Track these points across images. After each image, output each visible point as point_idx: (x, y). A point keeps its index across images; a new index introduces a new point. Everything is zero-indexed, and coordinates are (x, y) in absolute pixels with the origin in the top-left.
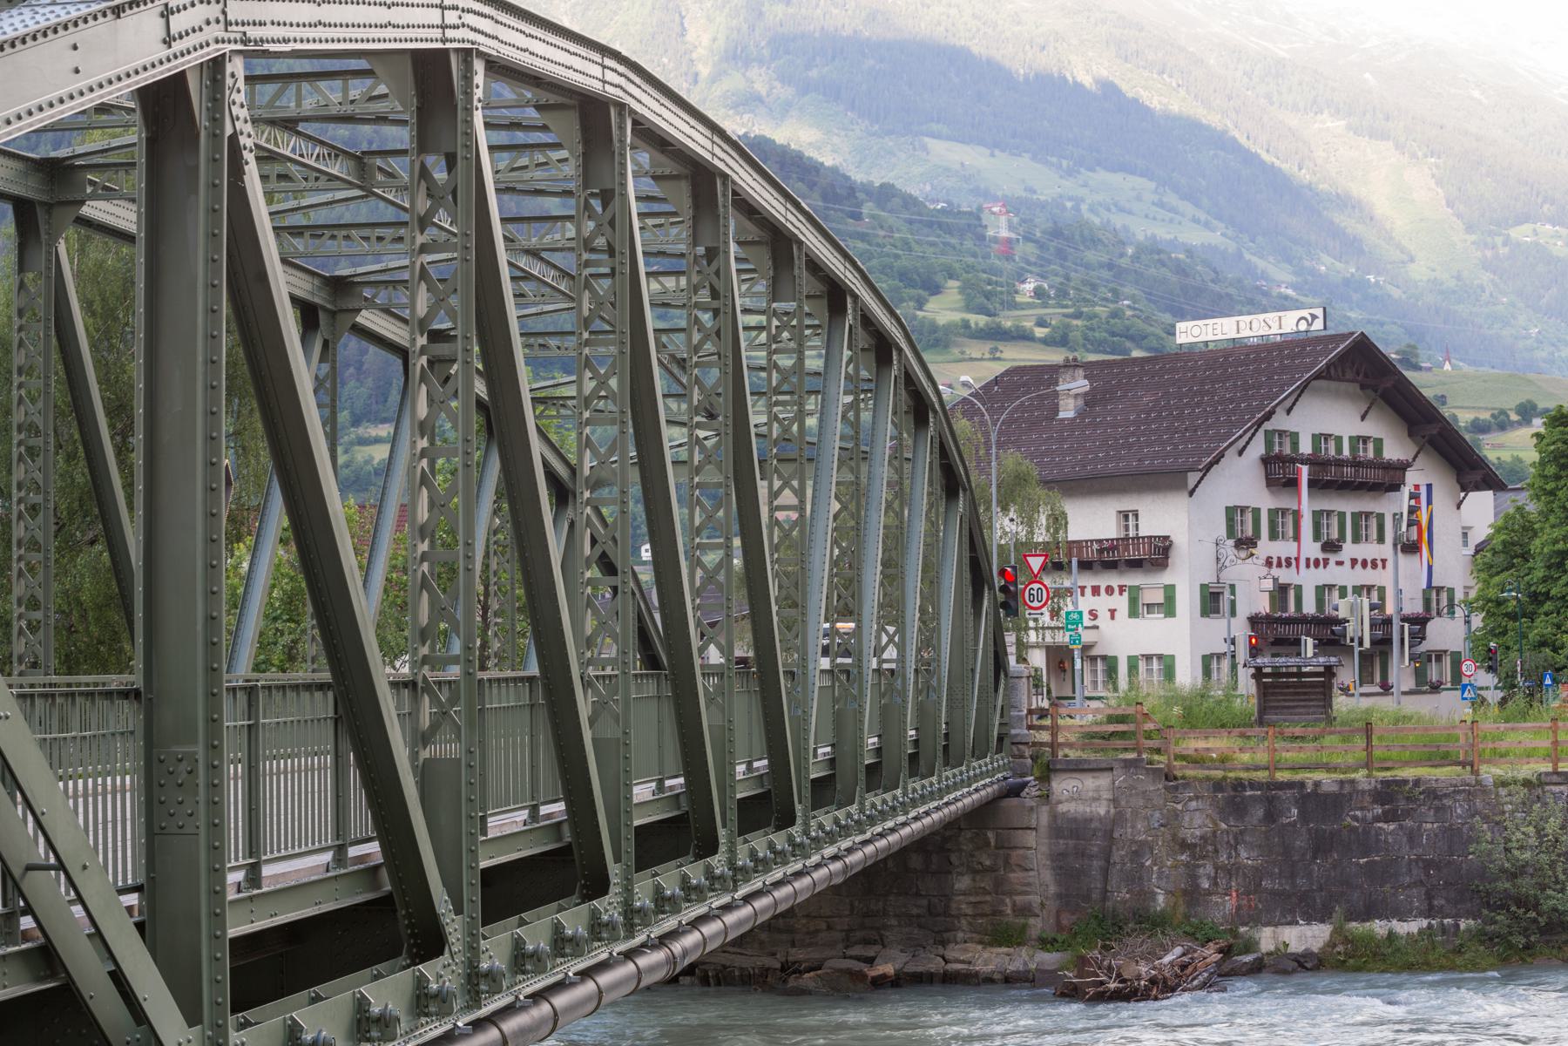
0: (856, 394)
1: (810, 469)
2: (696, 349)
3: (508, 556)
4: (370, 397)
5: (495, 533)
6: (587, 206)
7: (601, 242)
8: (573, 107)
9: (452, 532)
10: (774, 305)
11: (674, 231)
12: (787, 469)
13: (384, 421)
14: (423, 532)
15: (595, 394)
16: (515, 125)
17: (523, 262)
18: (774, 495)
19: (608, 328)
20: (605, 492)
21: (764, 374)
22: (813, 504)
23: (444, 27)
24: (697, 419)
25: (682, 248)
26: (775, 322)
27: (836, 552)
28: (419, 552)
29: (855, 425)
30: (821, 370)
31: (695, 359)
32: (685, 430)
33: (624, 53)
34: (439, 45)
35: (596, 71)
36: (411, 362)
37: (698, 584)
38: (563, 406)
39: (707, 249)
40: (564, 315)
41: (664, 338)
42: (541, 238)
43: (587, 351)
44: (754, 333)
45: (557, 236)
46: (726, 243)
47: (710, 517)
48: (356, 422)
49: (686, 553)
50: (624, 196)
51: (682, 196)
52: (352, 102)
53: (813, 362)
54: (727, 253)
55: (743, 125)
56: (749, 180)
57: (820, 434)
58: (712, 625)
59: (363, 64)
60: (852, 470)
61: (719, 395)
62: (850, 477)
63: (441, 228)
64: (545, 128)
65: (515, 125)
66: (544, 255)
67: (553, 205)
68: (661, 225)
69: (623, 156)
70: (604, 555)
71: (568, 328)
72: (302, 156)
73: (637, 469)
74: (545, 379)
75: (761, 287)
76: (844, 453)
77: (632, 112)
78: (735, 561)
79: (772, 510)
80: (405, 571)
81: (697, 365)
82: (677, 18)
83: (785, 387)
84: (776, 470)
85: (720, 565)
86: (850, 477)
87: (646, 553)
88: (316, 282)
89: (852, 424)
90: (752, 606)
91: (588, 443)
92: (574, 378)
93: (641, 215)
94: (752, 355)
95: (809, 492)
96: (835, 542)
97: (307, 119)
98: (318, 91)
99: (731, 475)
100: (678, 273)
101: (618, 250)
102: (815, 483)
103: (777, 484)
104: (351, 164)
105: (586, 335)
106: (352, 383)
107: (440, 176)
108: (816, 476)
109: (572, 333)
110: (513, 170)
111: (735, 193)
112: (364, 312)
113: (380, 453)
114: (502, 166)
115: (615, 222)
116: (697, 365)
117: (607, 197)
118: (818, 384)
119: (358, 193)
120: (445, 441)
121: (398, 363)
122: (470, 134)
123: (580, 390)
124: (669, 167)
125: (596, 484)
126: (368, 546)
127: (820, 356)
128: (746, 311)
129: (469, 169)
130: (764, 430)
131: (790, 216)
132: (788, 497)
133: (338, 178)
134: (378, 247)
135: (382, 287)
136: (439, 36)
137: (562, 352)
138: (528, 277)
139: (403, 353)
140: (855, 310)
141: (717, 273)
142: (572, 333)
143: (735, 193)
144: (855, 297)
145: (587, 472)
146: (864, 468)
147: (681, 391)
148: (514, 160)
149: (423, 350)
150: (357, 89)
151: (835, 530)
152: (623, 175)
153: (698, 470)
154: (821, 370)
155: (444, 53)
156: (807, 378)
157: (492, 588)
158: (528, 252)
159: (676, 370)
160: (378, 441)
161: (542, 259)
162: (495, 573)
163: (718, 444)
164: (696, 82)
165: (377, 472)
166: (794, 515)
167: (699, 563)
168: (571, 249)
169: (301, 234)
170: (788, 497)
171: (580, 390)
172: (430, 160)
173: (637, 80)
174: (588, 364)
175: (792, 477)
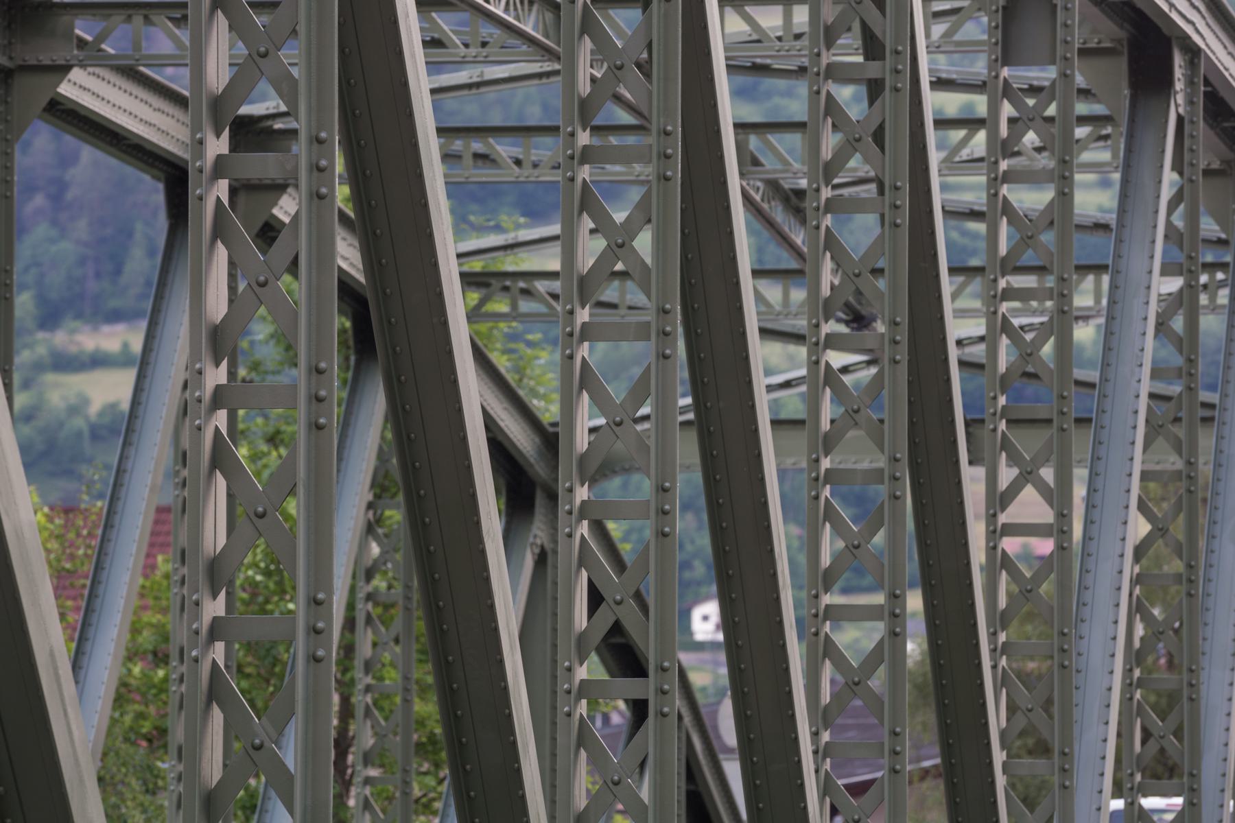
0: (1191, 275)
1: (1081, 443)
2: (829, 170)
3: (397, 626)
4: (82, 261)
5: (369, 575)
9: (278, 571)
10: (1005, 72)
12: (1029, 442)
13: (115, 316)
14: (217, 574)
15: (604, 271)
18: (999, 500)
19: (626, 118)
20: (613, 487)
21: (980, 227)
22: (1088, 522)
24: (831, 327)
26: (1007, 110)
27: (1139, 630)
28: (206, 619)
29: (1188, 343)
30: (1112, 219)
31: (826, 193)
32: (802, 352)
36: (194, 191)
37: (826, 697)
38: (526, 292)
40: (532, 86)
41: (753, 142)
43: (585, 173)
44: (958, 134)
47: (854, 548)
48: (50, 318)
49: (799, 622)
53: (1093, 199)
57: (1106, 365)
58: (858, 790)
60: (1178, 447)
61: (878, 272)
62: (1174, 462)
70: (617, 628)
71: (534, 117)
73: (693, 435)
74: (481, 230)
75: (976, 29)
76: (1161, 408)
78: (910, 646)
79: (995, 533)
80: (160, 658)
81: (830, 206)
83: (1028, 258)
84: (1006, 445)
85: (874, 659)
86: (1174, 462)
87: (705, 621)
89: (1179, 343)
90: (947, 750)
91: (587, 380)
92: (555, 229)
94: (954, 187)
95: (1079, 492)
96: (1138, 608)
99: (903, 454)
102: (1093, 475)
103: (1006, 475)
105: (584, 138)
106: (41, 230)
108: (1096, 458)
109: (554, 130)
112: (76, 74)
113: (110, 390)
116: (830, 206)
118: (1093, 251)
120: (255, 366)
121: (153, 192)
123: (569, 256)
125: (599, 468)
126: (83, 594)
127: (1105, 184)
128: (940, 84)
130: (978, 352)
132: (1030, 506)
135: (118, 18)
137: (526, 173)
139: (175, 177)
140: (1190, 82)
142: (554, 130)
144: (1193, 53)
145: (582, 441)
146: (1206, 440)
147: (794, 265)
149: (220, 168)
151: (1137, 580)
153: (829, 443)
154: (1112, 219)
156: (1077, 236)
157: (360, 700)
159: (779, 214)
160: (98, 361)
162: (368, 667)
163: (878, 379)
165: (97, 433)
166: (1045, 546)
167: (829, 650)
170: (1030, 506)
171: (569, 256)
174: (588, 202)
175: (1038, 461)
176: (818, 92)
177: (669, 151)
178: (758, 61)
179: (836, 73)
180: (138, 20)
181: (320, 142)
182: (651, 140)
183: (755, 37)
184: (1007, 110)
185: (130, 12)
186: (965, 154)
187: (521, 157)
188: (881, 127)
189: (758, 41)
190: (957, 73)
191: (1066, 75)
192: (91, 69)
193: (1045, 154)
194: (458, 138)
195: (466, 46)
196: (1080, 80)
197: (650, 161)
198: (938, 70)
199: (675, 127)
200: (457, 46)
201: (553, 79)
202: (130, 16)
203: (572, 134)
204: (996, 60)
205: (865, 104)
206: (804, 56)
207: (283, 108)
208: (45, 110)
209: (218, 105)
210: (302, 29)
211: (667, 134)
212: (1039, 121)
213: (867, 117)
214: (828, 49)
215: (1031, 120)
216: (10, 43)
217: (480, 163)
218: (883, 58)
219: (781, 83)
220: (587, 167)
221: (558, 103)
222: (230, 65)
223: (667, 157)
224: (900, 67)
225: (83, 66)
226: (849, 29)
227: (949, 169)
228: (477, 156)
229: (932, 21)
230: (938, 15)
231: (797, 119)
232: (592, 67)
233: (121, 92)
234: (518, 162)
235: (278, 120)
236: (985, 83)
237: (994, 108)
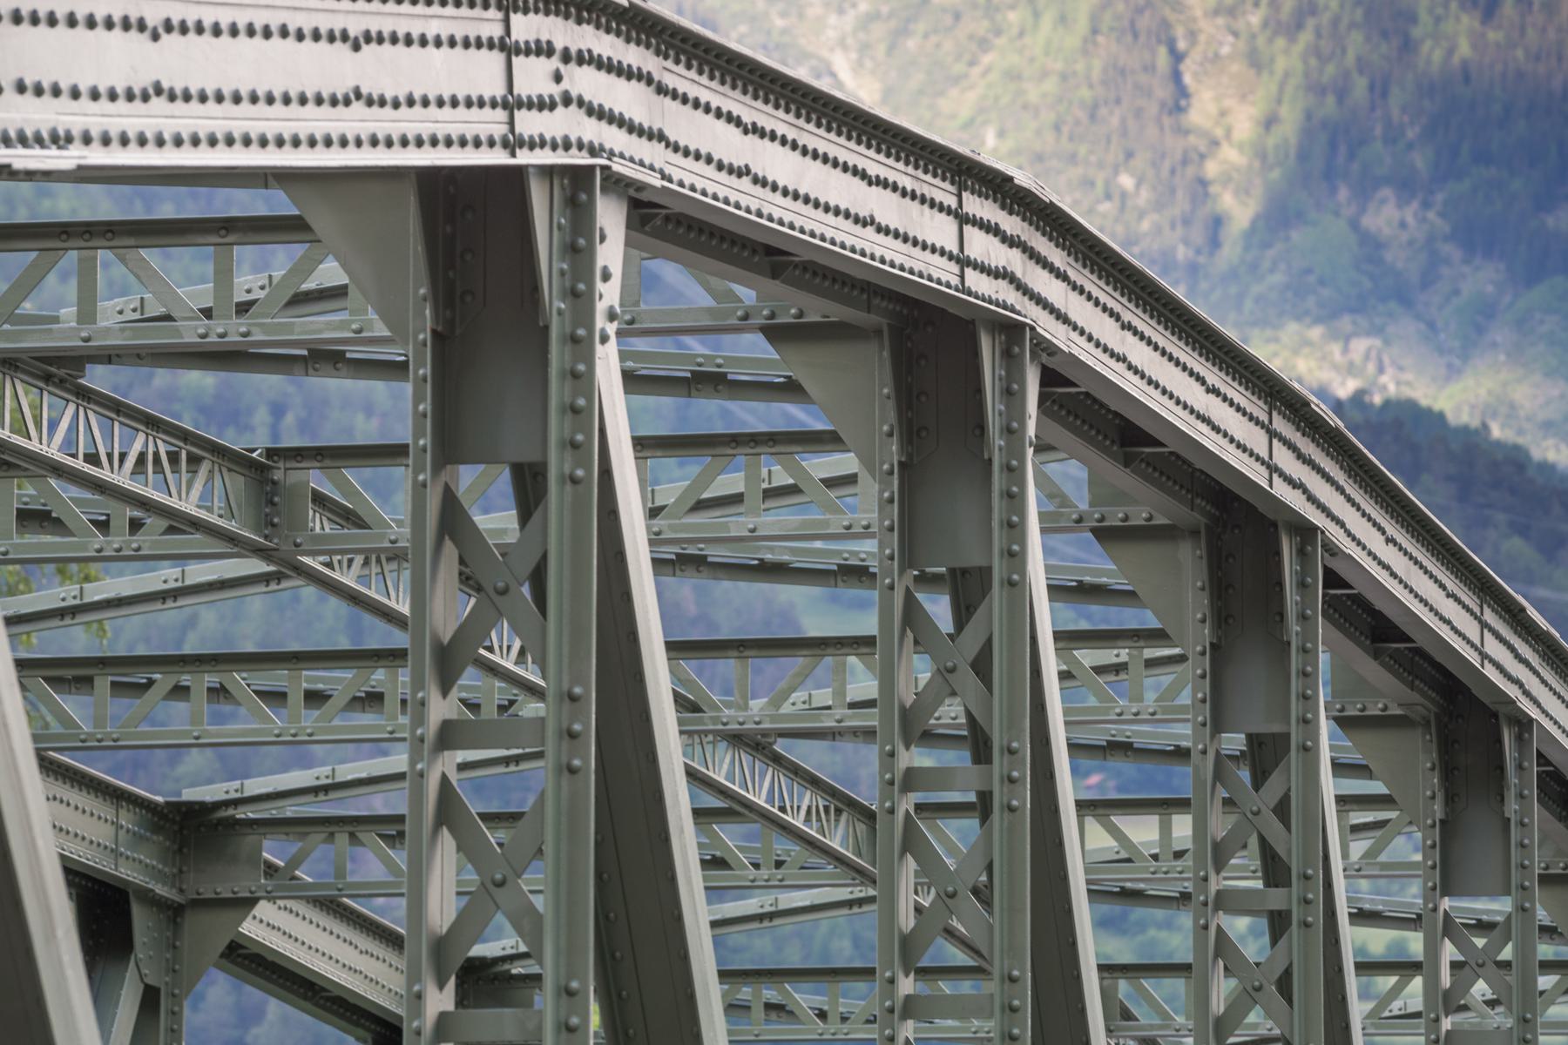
6: (913, 615)
7: (950, 713)
8: (878, 332)
10: (1446, 903)
11: (1166, 678)
16: (708, 381)
17: (723, 767)
19: (960, 958)
23: (511, 104)
25: (1182, 733)
26: (1449, 951)
32: (1185, 919)
33: (1022, 178)
34: (498, 158)
35: (941, 231)
39: (1250, 737)
41: (1123, 987)
42: (777, 702)
45: (823, 696)
46: (1308, 723)
50: (1017, 586)
51: (1177, 589)
52: (244, 308)
54: (1309, 751)
55: (1351, 369)
56: (1375, 542)
59: (278, 203)
63: (493, 670)
64: (791, 389)
65: (708, 381)
66: (780, 746)
67: (813, 612)
68: (1118, 668)
69: (1014, 473)
71: (844, 954)
72: (93, 459)
75: (1408, 847)
77: (1043, 347)
82: (1162, 58)
88: (127, 819)
93: (1065, 638)
97: (108, 357)
98: (145, 275)
100: (1167, 806)
101: (998, 743)
104: (237, 483)
105: (907, 985)
107: (497, 521)
109: (868, 973)
110: (701, 506)
111: (1332, 579)
112: (264, 909)
114: (668, 494)
115: (992, 668)
117: (968, 587)
119: (257, 566)
122: (584, 411)
124: (1146, 504)
128: (1363, 917)
129: (580, 507)
131: (1493, 647)
133: (196, 524)
134: (310, 719)
135: (317, 837)
136: (499, 130)
137: (832, 1028)
138: (734, 809)
141: (1282, 810)
142: (868, 973)
143: (1332, 579)
148: (705, 479)
150: (258, 271)
152: (1016, 529)
155: (516, 176)
158: (737, 739)
161: (777, 760)
164: (1214, 242)
168: (869, 734)
169: (83, 683)
172: (466, 477)
173: (1057, 257)
176: (1206, 927)
177: (1016, 1003)
178: (1128, 885)
179: (1227, 902)
180: (342, 839)
181: (570, 993)
182: (991, 987)
183: (1124, 855)
184: (1449, 951)
185: (331, 829)
186: (1396, 1007)
187: (826, 1008)
188: (1288, 973)
189: (1129, 860)
190: (1384, 903)
191: (1524, 910)
192: (281, 903)
193: (1500, 1009)
194: (745, 984)
195: (756, 866)
196: (1542, 915)
197: (991, 1016)
198: (1360, 899)
199: (1023, 971)
200: (746, 867)
201: (865, 908)
202: (332, 834)
203: (892, 981)
204: (1434, 888)
205: (1266, 939)
206: (1187, 879)
207: (523, 948)
208: (222, 955)
209: (440, 946)
210: (548, 849)
211: (1012, 980)
212: (1491, 967)
213: (1270, 959)
214: (1218, 872)
215: (1481, 966)
216: (181, 871)
217: (773, 1016)
218: (1288, 884)
219: (1159, 913)
220: (910, 1023)
221: (872, 936)
222: (459, 893)
223: (1013, 1010)
224: (1310, 896)
225: (272, 899)
226: (1245, 846)
227: (1376, 1026)
228: (769, 1007)
229: (1350, 837)
230: (1356, 829)
231: (1177, 960)
232: (916, 893)
233: (319, 931)
234: (822, 1015)
235: (517, 963)
236: (1419, 916)
237: (1432, 949)
